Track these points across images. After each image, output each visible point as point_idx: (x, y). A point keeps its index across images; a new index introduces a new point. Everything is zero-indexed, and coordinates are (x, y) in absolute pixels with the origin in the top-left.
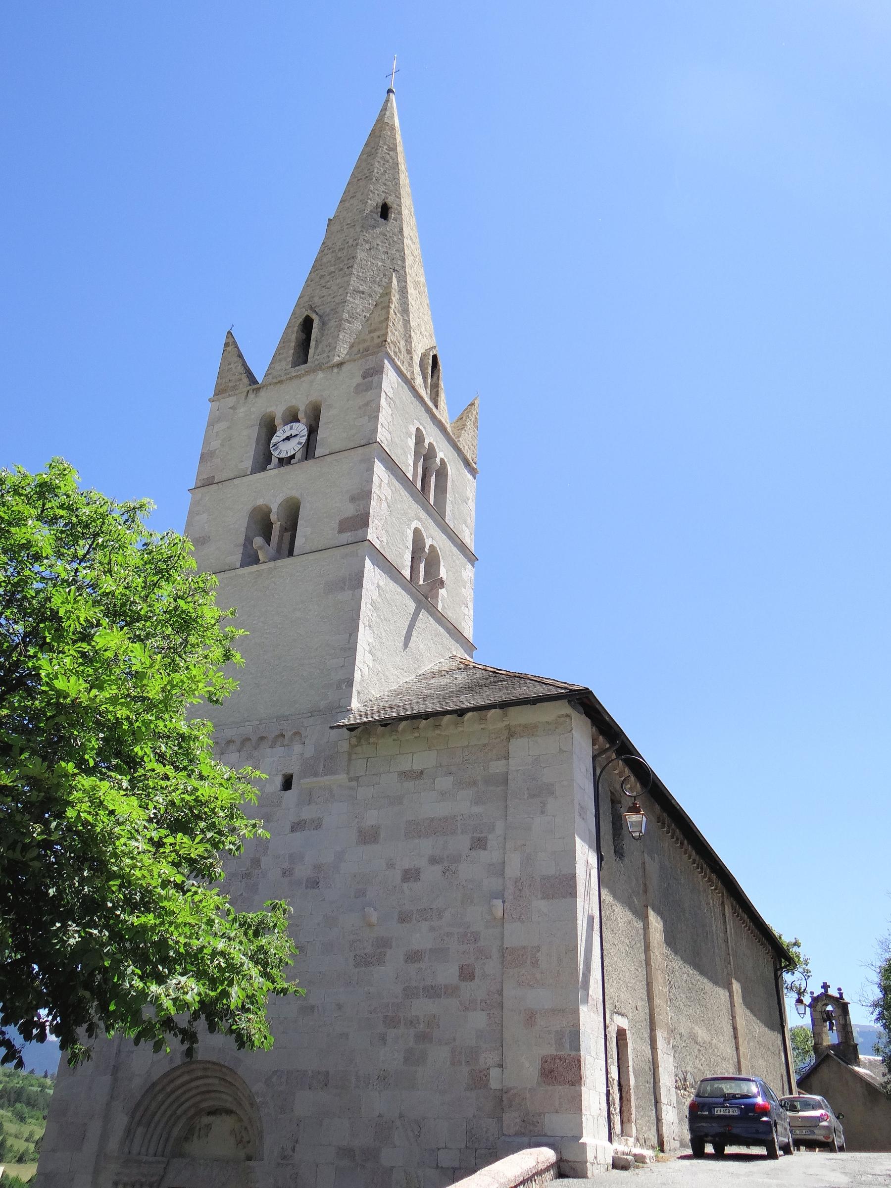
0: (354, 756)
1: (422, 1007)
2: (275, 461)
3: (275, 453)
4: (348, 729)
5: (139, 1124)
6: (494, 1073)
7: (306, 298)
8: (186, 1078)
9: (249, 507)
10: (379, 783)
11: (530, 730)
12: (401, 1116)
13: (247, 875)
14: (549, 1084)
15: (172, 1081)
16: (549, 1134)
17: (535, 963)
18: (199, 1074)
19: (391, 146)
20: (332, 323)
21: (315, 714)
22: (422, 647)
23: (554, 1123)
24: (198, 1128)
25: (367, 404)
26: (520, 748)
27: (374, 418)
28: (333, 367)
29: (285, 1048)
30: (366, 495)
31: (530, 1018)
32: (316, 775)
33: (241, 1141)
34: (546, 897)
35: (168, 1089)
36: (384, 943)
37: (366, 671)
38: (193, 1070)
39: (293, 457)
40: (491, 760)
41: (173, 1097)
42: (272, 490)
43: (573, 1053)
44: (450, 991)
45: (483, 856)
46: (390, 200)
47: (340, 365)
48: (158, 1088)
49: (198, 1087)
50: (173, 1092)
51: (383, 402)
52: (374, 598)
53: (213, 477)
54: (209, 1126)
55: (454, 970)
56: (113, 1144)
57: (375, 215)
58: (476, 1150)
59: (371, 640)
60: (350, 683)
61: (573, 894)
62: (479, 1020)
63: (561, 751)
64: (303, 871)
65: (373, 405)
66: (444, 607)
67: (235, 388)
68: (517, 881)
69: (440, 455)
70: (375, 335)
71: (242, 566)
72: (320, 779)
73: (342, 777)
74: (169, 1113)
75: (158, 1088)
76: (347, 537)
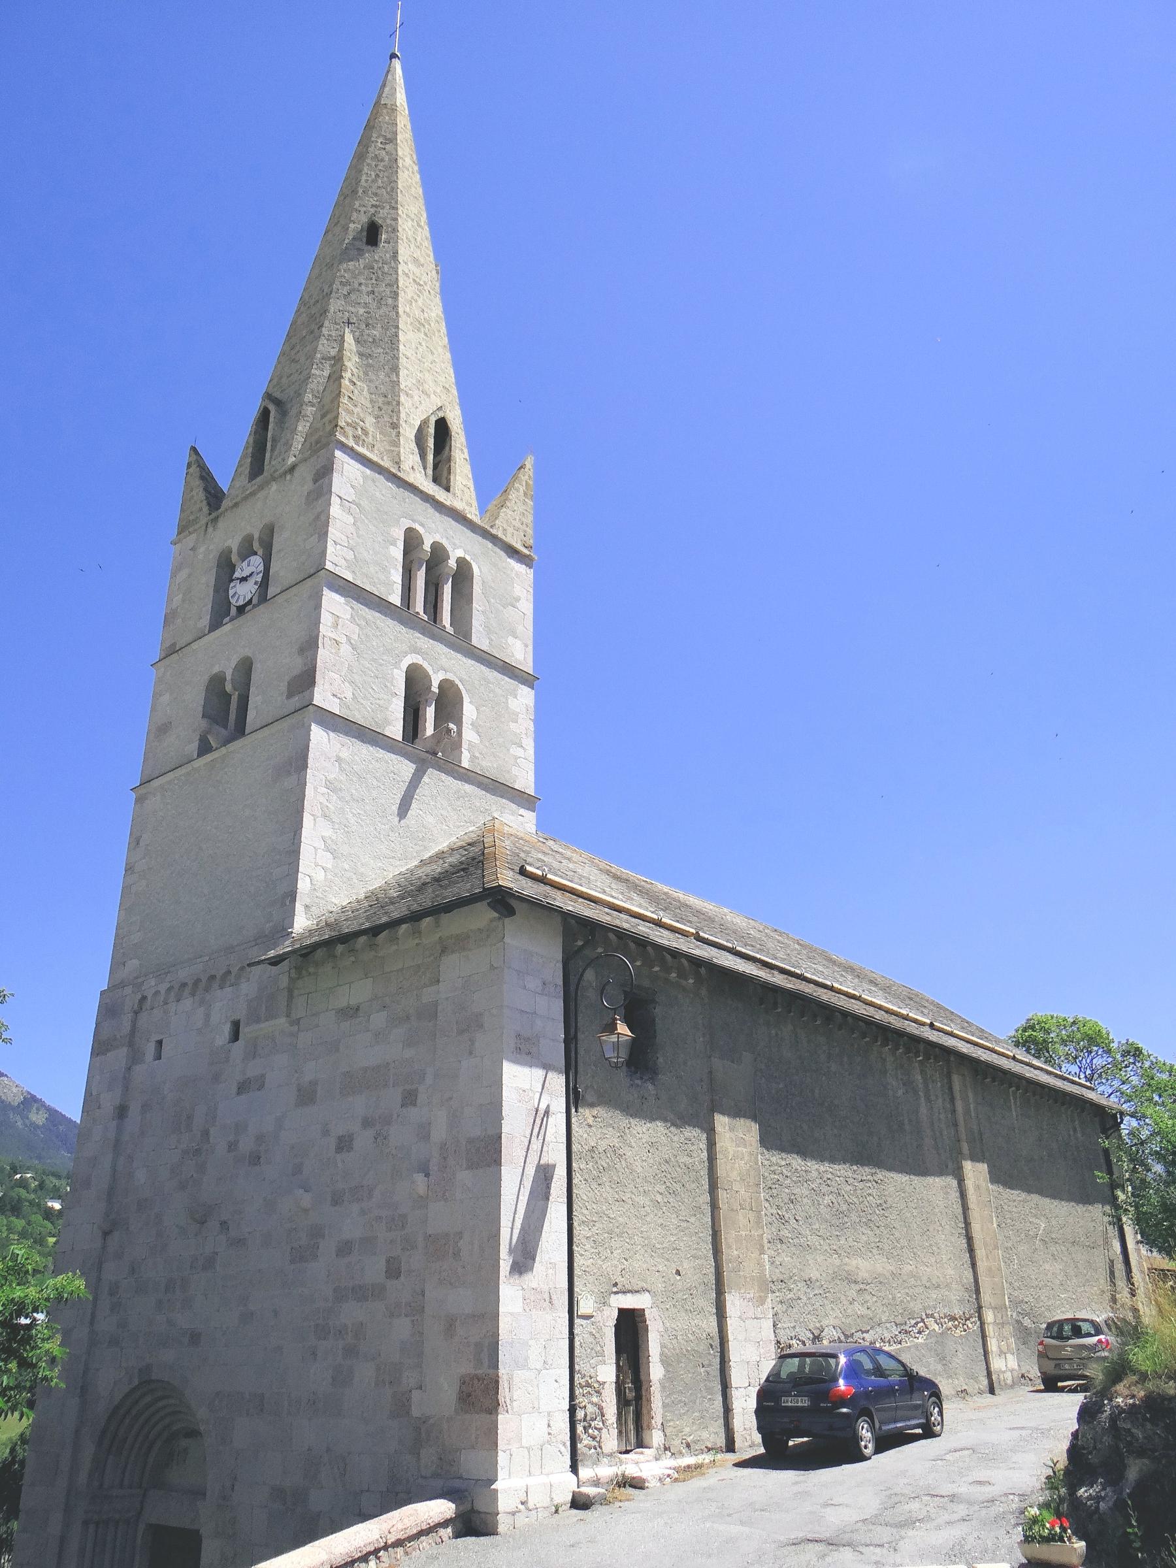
0: (296, 992)
1: (352, 1313)
2: (233, 611)
3: (233, 601)
4: (301, 956)
6: (416, 1395)
7: (275, 382)
8: (148, 1399)
9: (206, 678)
10: (318, 1026)
11: (460, 943)
12: (328, 1450)
13: (197, 1152)
14: (466, 1412)
16: (465, 1475)
17: (457, 1255)
19: (389, 136)
20: (293, 412)
21: (259, 941)
22: (430, 819)
23: (470, 1463)
25: (318, 517)
26: (454, 968)
27: (322, 533)
28: (285, 473)
30: (310, 645)
31: (450, 1326)
32: (258, 1021)
34: (470, 1167)
35: (134, 1412)
36: (317, 1233)
37: (320, 876)
39: (250, 602)
40: (425, 986)
42: (220, 653)
43: (491, 1371)
44: (378, 1292)
45: (413, 1113)
46: (381, 217)
47: (293, 468)
51: (335, 510)
52: (331, 777)
53: (174, 644)
55: (382, 1265)
56: (82, 1478)
57: (358, 244)
58: (397, 1494)
59: (328, 833)
60: (292, 895)
61: (498, 1162)
62: (402, 1328)
63: (492, 968)
64: (246, 1145)
65: (323, 518)
66: (473, 758)
67: (196, 521)
68: (443, 1146)
69: (455, 554)
70: (326, 419)
71: (199, 756)
72: (262, 1025)
73: (282, 1021)
76: (296, 702)
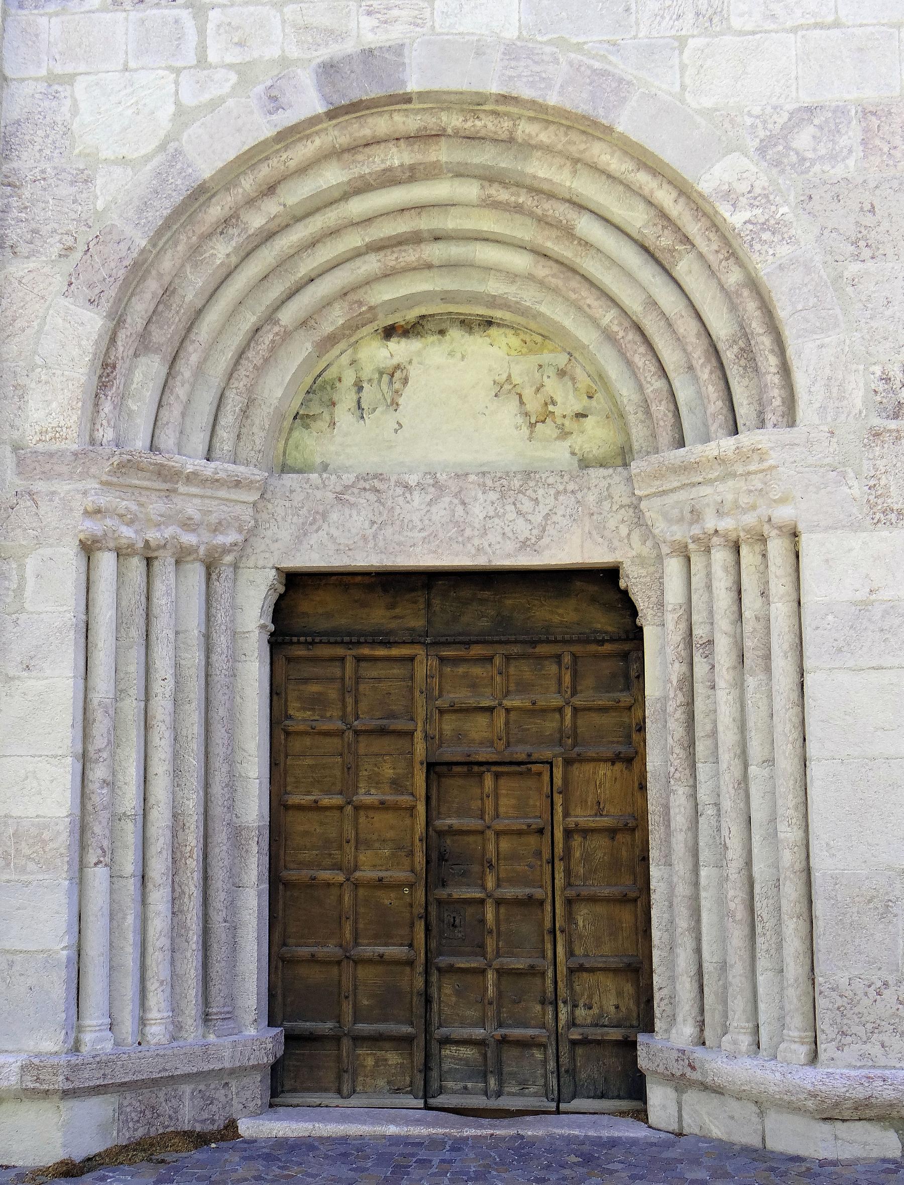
5: (144, 344)
8: (332, 176)
15: (271, 189)
18: (397, 157)
24: (349, 378)
29: (837, 24)
33: (545, 416)
35: (256, 221)
38: (168, 292)
41: (267, 257)
48: (215, 212)
49: (367, 221)
50: (268, 236)
54: (395, 375)
74: (248, 320)
75: (215, 212)
